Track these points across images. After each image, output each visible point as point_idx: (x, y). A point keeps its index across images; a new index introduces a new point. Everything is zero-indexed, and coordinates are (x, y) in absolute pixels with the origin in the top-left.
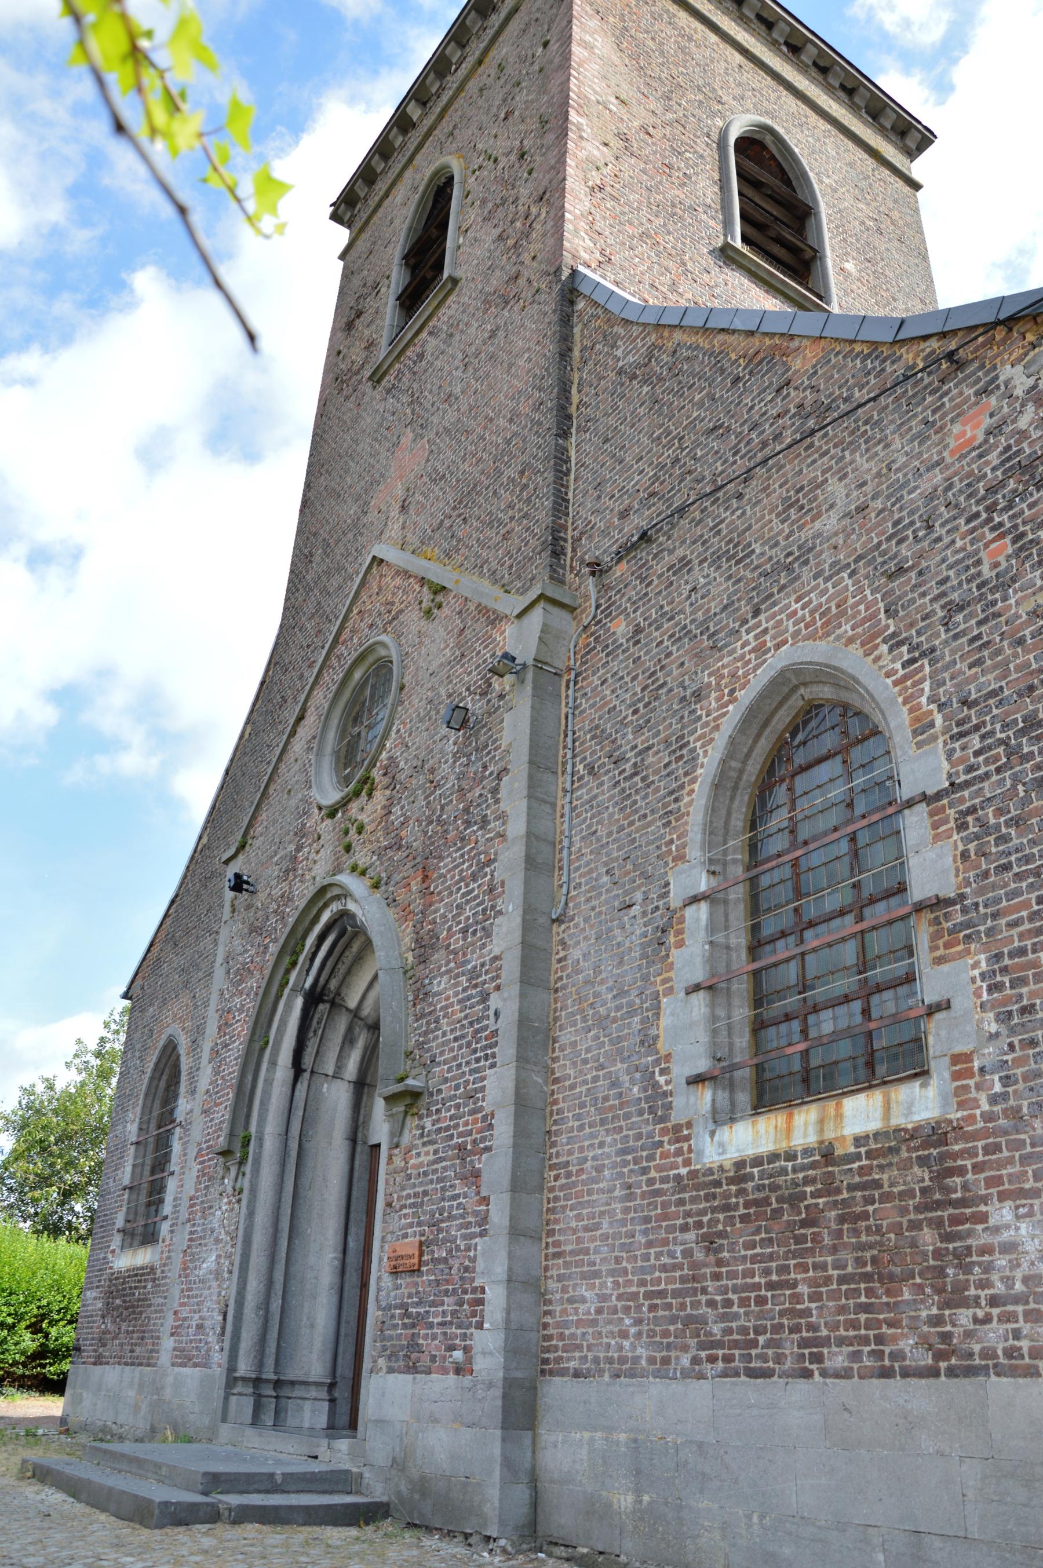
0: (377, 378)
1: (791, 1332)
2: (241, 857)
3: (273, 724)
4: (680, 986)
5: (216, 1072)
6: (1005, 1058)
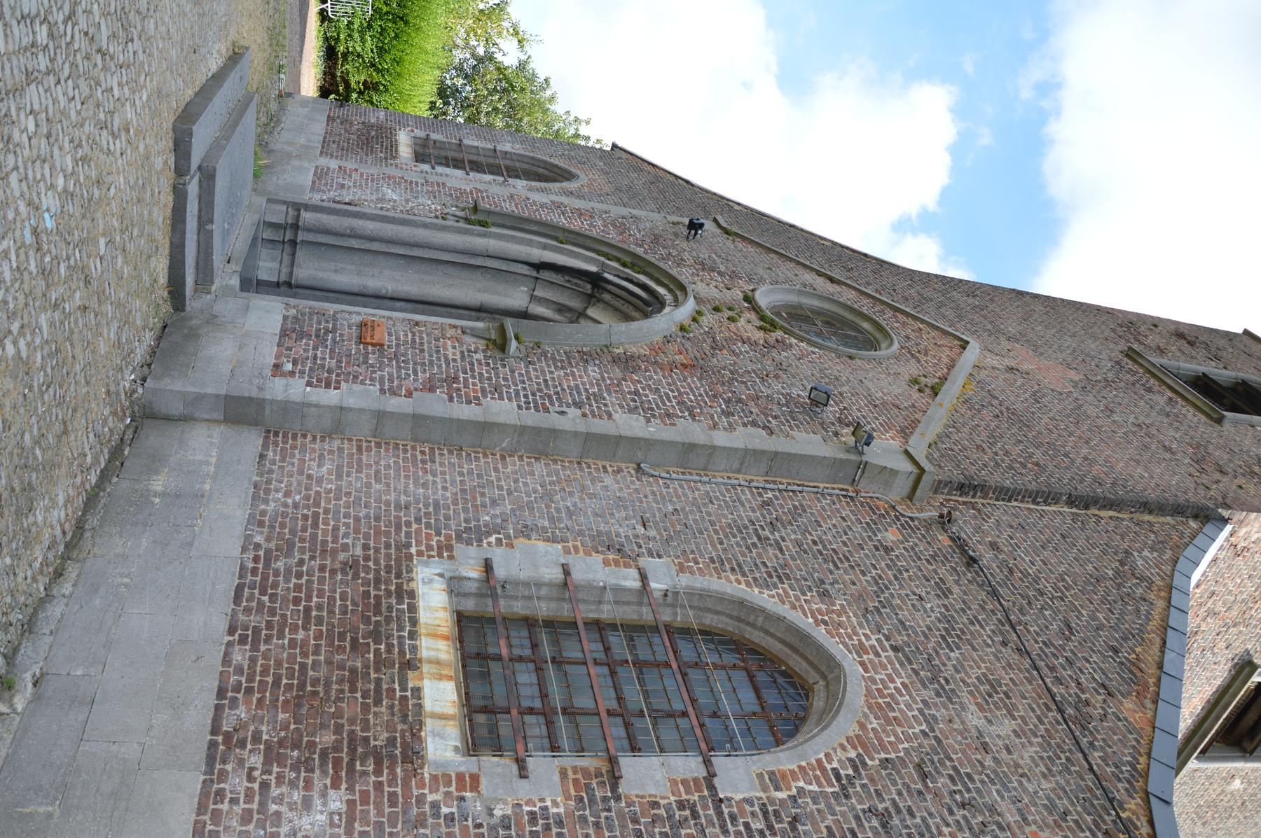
0: (1131, 354)
1: (268, 622)
2: (718, 231)
3: (829, 261)
4: (569, 559)
5: (542, 206)
6: (470, 819)
